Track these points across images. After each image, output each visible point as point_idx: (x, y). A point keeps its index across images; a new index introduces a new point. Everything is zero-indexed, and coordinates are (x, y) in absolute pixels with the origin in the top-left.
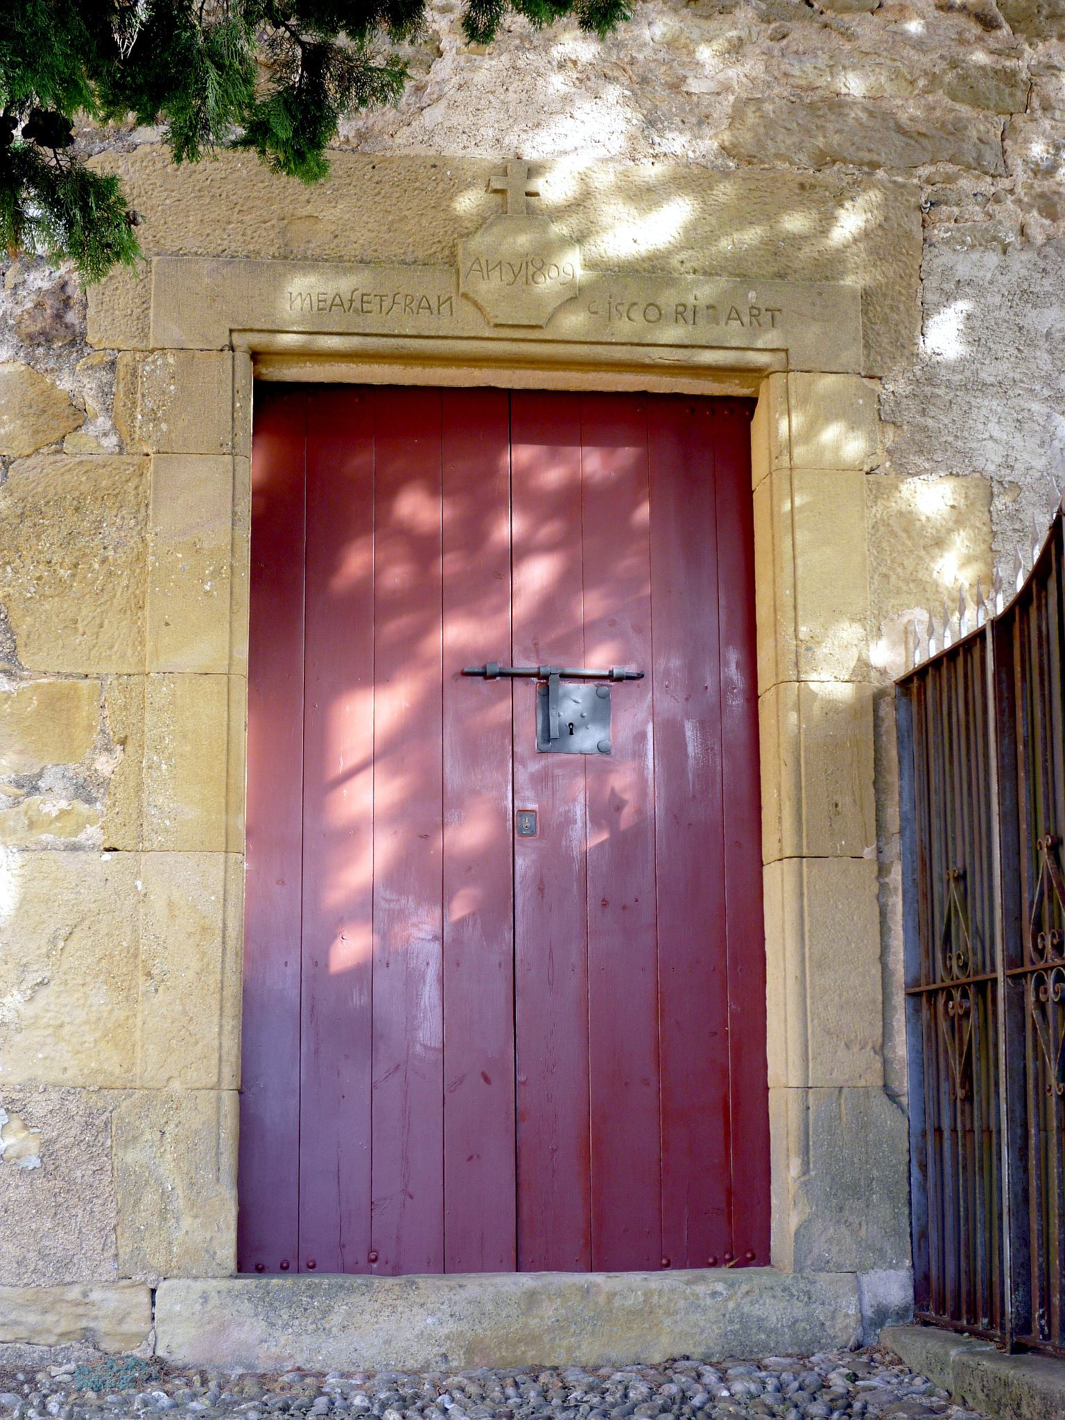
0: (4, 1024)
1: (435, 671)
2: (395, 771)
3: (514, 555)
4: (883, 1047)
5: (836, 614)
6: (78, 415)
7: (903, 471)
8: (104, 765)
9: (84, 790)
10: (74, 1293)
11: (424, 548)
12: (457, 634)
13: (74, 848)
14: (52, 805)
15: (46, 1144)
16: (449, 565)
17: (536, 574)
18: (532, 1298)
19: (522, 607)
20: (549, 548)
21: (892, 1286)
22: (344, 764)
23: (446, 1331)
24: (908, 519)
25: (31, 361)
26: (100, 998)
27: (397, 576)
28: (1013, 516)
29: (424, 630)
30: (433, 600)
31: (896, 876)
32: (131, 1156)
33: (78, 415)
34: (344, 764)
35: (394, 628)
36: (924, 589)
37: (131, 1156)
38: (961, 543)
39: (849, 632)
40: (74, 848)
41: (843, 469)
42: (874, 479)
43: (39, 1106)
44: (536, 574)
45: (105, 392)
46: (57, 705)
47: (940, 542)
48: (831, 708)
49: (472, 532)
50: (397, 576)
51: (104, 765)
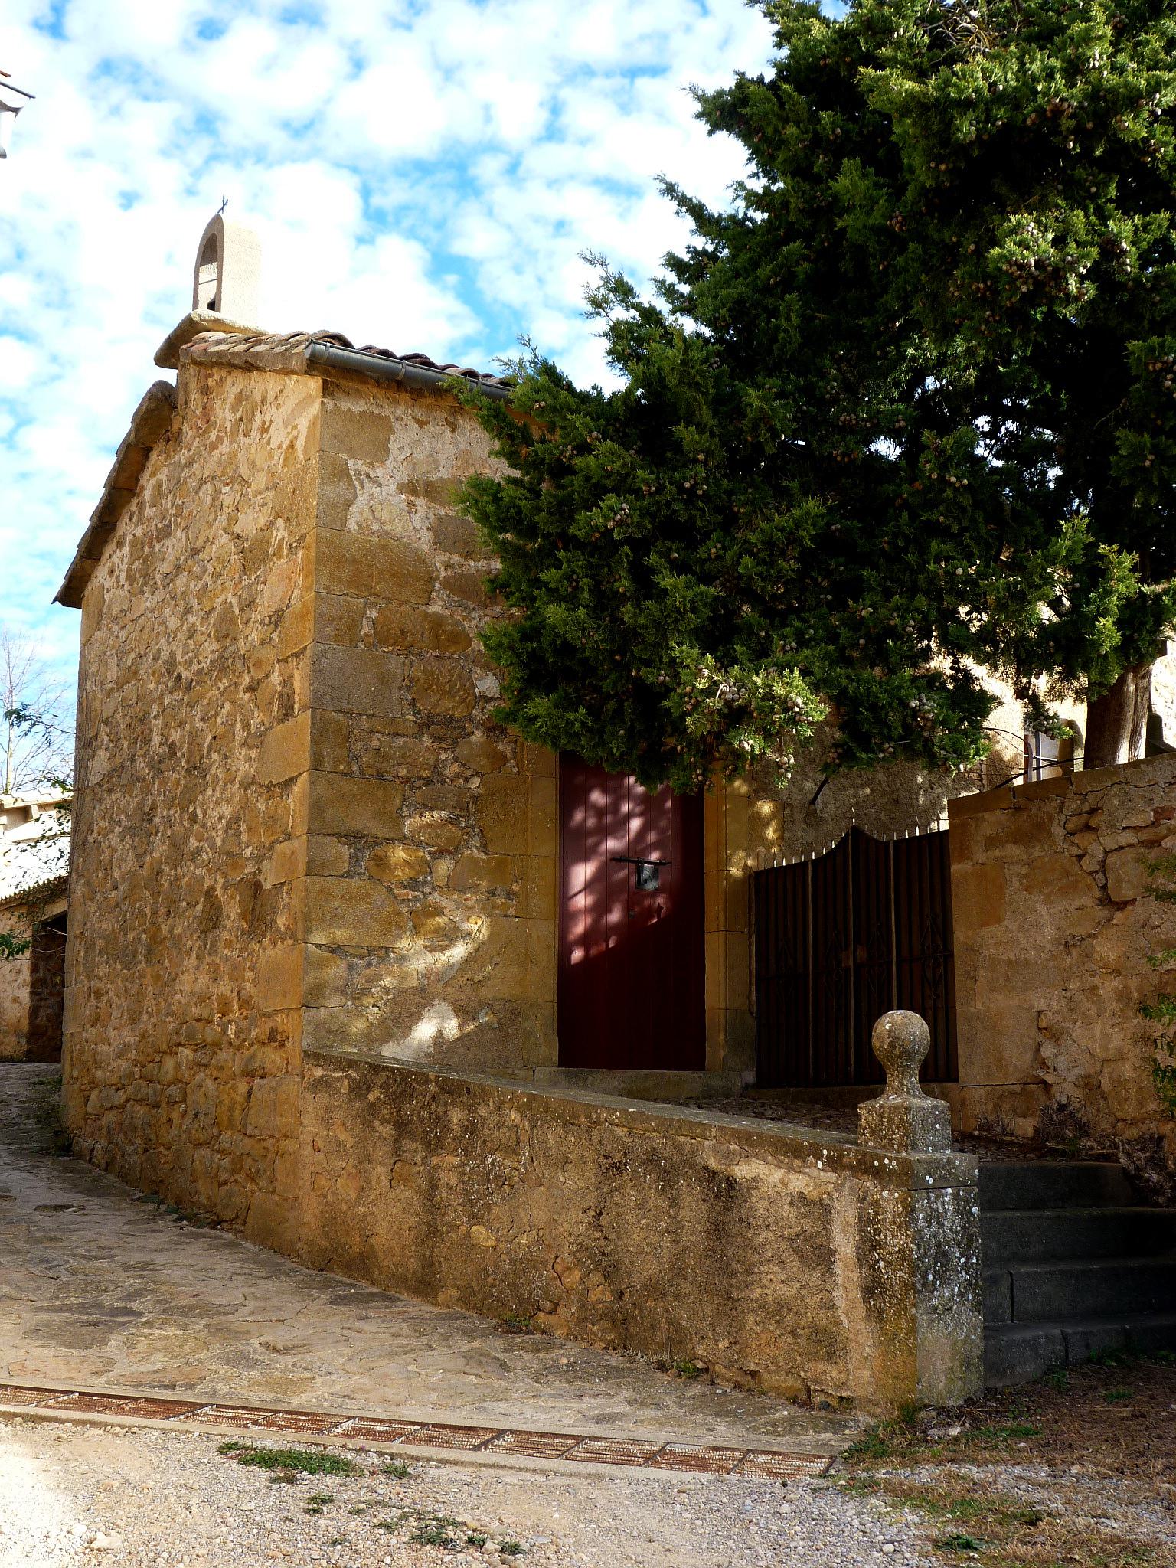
0: (1165, 896)
1: (603, 858)
2: (590, 893)
3: (629, 816)
4: (749, 997)
5: (738, 847)
6: (504, 759)
7: (759, 798)
8: (515, 887)
9: (509, 896)
10: (510, 1071)
11: (600, 812)
12: (611, 844)
13: (506, 916)
14: (500, 901)
15: (499, 1020)
16: (608, 819)
17: (635, 824)
18: (646, 1076)
19: (632, 834)
20: (640, 815)
21: (750, 1077)
22: (573, 892)
23: (1049, 932)
24: (759, 813)
25: (488, 737)
26: (515, 969)
27: (591, 822)
28: (791, 816)
29: (599, 843)
30: (604, 832)
31: (754, 939)
32: (527, 1024)
33: (504, 759)
34: (573, 892)
35: (591, 841)
36: (763, 840)
37: (527, 1024)
38: (774, 824)
39: (741, 854)
40: (506, 916)
41: (741, 796)
42: (751, 799)
43: (497, 1007)
44: (635, 824)
45: (513, 751)
46: (501, 864)
47: (767, 824)
48: (736, 880)
49: (615, 807)
50: (591, 822)
51: (515, 887)
